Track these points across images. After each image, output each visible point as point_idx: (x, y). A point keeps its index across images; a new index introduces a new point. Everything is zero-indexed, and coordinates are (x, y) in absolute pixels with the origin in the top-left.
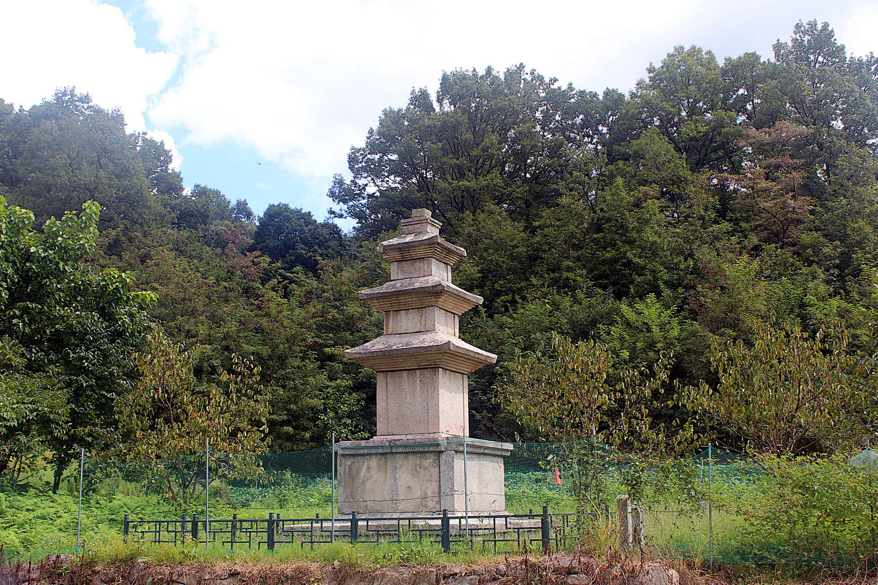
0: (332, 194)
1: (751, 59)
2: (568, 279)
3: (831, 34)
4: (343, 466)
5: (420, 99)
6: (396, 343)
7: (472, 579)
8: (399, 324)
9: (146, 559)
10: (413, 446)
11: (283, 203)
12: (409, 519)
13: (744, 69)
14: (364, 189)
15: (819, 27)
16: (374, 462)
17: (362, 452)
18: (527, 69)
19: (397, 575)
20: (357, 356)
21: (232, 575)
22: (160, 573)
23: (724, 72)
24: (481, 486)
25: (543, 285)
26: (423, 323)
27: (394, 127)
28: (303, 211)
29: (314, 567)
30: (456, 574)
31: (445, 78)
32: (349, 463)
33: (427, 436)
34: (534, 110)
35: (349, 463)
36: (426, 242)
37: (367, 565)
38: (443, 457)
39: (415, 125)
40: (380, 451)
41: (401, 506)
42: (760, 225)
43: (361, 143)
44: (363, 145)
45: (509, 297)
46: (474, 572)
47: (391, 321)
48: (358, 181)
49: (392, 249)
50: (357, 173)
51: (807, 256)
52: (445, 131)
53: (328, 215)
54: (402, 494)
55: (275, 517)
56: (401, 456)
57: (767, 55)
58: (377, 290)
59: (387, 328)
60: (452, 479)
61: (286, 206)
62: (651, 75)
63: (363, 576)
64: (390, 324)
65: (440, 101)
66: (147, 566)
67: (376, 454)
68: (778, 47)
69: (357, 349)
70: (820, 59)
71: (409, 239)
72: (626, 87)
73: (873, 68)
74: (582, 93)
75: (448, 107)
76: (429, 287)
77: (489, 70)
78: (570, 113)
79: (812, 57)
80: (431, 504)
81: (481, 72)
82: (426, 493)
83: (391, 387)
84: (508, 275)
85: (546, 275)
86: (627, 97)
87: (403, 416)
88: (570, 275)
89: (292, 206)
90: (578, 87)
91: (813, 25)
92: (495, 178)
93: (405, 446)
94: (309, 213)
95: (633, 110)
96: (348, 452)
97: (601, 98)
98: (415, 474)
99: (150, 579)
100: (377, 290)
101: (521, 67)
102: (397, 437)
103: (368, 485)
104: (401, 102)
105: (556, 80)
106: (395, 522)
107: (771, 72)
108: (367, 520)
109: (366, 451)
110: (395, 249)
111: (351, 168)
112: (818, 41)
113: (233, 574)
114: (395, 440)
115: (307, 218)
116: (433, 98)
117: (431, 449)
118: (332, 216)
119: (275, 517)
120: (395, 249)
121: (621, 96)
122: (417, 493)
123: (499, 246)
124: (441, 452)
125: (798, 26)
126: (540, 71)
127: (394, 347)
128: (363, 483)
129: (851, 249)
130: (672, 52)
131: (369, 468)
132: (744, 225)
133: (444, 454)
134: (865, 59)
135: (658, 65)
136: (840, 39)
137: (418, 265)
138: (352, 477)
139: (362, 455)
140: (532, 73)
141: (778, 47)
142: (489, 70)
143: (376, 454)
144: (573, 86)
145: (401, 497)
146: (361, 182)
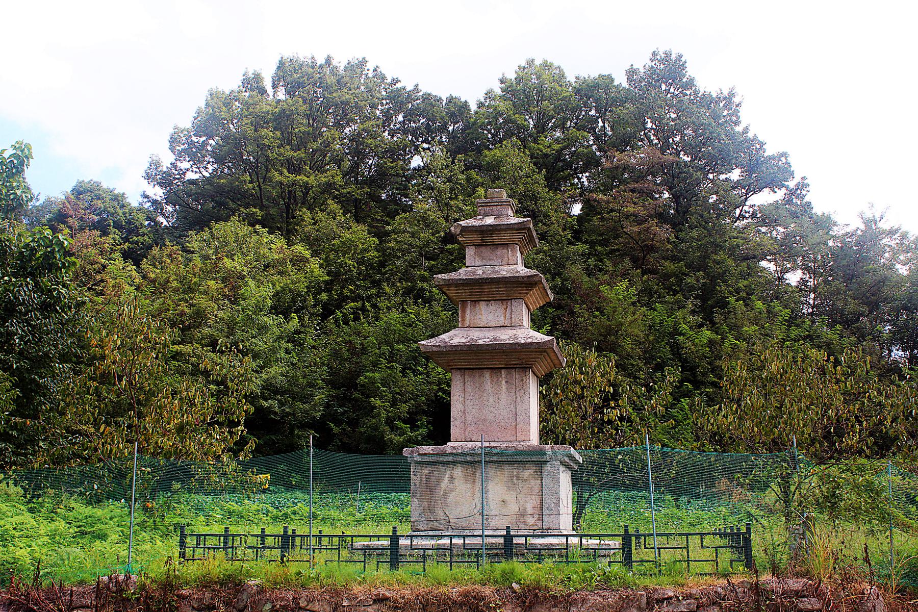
0: (148, 177)
1: (605, 82)
2: (422, 289)
3: (683, 67)
4: (417, 477)
5: (253, 83)
6: (483, 337)
7: (689, 604)
8: (478, 316)
9: (258, 581)
10: (511, 455)
11: (95, 180)
12: (526, 536)
13: (595, 92)
14: (184, 173)
15: (673, 57)
16: (458, 472)
17: (445, 459)
18: (370, 66)
19: (600, 599)
20: (435, 349)
21: (378, 600)
22: (282, 599)
23: (577, 91)
24: (554, 505)
25: (396, 294)
26: (508, 317)
27: (224, 109)
28: (116, 192)
29: (487, 591)
30: (671, 598)
31: (281, 65)
32: (426, 472)
33: (515, 444)
34: (373, 106)
35: (426, 472)
36: (516, 226)
37: (558, 589)
38: (547, 468)
39: (251, 110)
40: (469, 458)
41: (494, 522)
42: (618, 250)
43: (186, 122)
44: (189, 125)
45: (359, 304)
46: (690, 596)
47: (468, 312)
48: (178, 164)
49: (470, 231)
50: (180, 156)
51: (673, 285)
52: (281, 120)
53: (141, 199)
54: (493, 507)
55: (290, 533)
56: (494, 466)
57: (621, 80)
58: (453, 275)
59: (463, 320)
60: (557, 493)
61: (98, 184)
62: (503, 85)
63: (555, 600)
64: (468, 316)
65: (275, 86)
66: (261, 590)
67: (461, 462)
68: (631, 73)
69: (434, 341)
70: (672, 90)
71: (489, 221)
72: (473, 97)
73: (721, 105)
74: (427, 97)
75: (281, 95)
76: (523, 277)
77: (328, 61)
78: (410, 115)
79: (664, 87)
80: (531, 521)
81: (321, 61)
82: (525, 510)
83: (469, 388)
84: (359, 280)
85: (399, 284)
86: (473, 107)
87: (485, 420)
88: (425, 285)
89: (105, 185)
90: (424, 89)
91: (668, 54)
92: (334, 175)
93: (502, 454)
94: (123, 194)
95: (482, 120)
96: (426, 459)
97: (444, 102)
98: (511, 485)
99: (268, 606)
100: (453, 275)
101: (363, 63)
102: (493, 444)
103: (451, 498)
104: (230, 83)
105: (398, 81)
106: (564, 540)
107: (623, 98)
108: (451, 537)
109: (450, 459)
110: (476, 231)
111: (172, 149)
112: (669, 70)
113: (380, 600)
114: (491, 447)
115: (118, 199)
116: (268, 84)
117: (534, 459)
118: (145, 200)
119: (290, 533)
120: (476, 231)
121: (465, 105)
122: (513, 508)
123: (346, 247)
124: (546, 462)
125: (654, 54)
126: (384, 70)
127: (481, 342)
128: (445, 495)
129: (713, 279)
130: (523, 64)
131: (452, 478)
132: (599, 248)
133: (548, 465)
134: (714, 96)
135: (511, 76)
136: (691, 71)
137: (500, 251)
138: (430, 488)
139: (448, 463)
140: (375, 70)
141: (631, 73)
142: (328, 61)
143: (461, 462)
144: (420, 87)
145: (493, 512)
146: (185, 165)
